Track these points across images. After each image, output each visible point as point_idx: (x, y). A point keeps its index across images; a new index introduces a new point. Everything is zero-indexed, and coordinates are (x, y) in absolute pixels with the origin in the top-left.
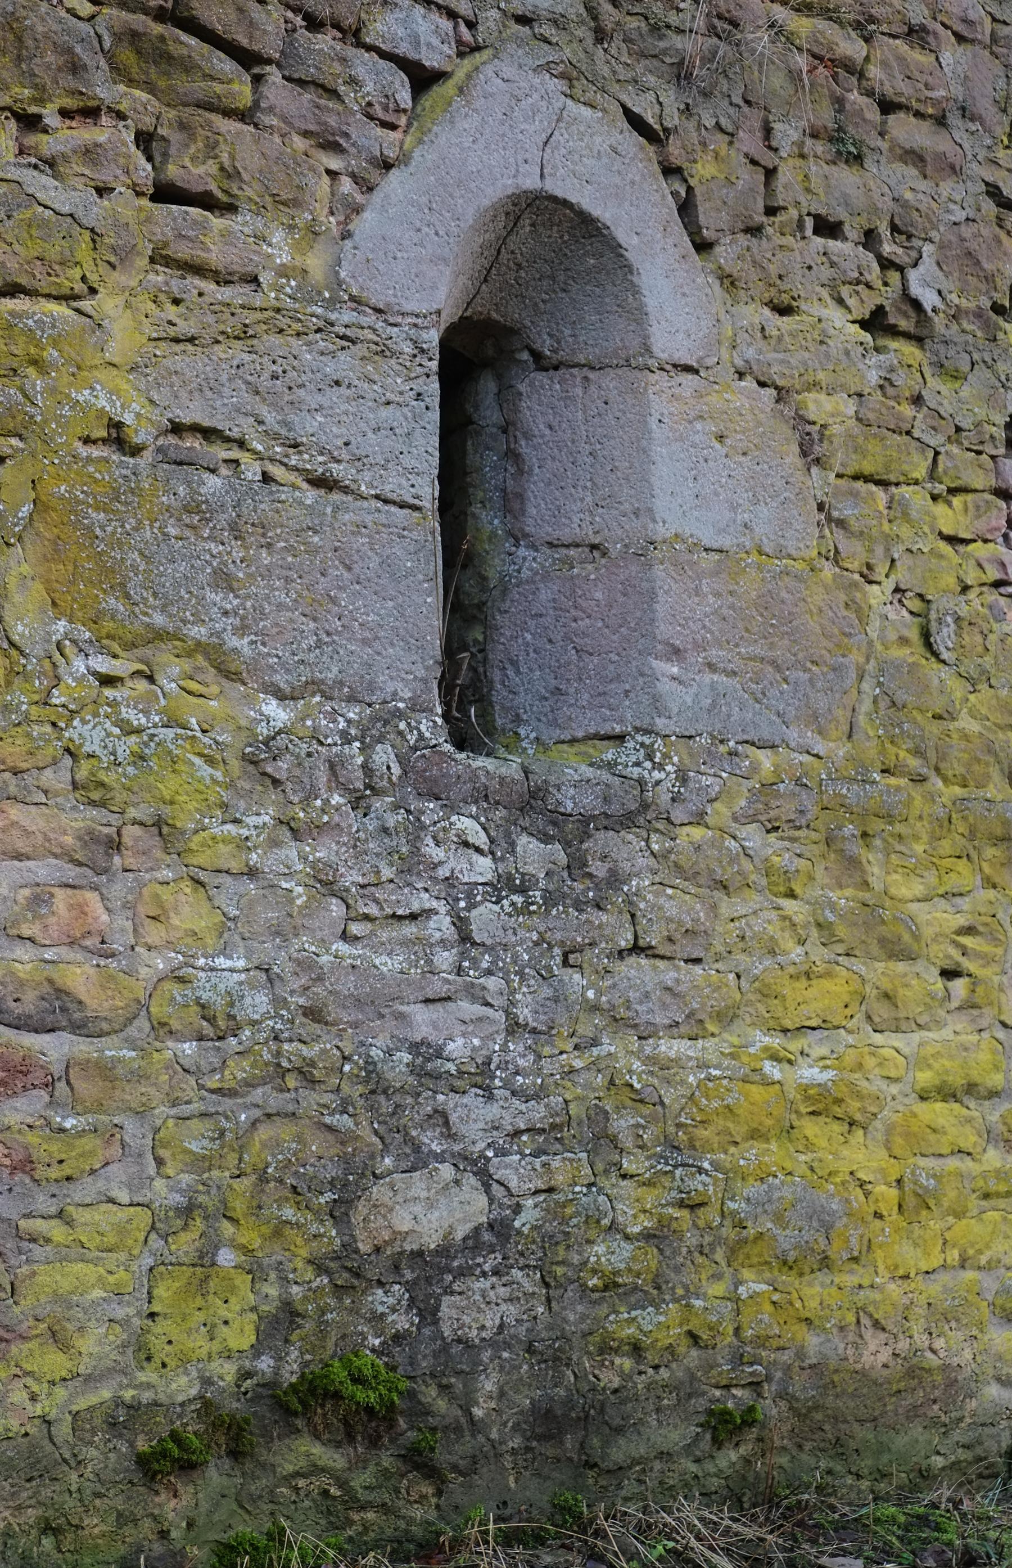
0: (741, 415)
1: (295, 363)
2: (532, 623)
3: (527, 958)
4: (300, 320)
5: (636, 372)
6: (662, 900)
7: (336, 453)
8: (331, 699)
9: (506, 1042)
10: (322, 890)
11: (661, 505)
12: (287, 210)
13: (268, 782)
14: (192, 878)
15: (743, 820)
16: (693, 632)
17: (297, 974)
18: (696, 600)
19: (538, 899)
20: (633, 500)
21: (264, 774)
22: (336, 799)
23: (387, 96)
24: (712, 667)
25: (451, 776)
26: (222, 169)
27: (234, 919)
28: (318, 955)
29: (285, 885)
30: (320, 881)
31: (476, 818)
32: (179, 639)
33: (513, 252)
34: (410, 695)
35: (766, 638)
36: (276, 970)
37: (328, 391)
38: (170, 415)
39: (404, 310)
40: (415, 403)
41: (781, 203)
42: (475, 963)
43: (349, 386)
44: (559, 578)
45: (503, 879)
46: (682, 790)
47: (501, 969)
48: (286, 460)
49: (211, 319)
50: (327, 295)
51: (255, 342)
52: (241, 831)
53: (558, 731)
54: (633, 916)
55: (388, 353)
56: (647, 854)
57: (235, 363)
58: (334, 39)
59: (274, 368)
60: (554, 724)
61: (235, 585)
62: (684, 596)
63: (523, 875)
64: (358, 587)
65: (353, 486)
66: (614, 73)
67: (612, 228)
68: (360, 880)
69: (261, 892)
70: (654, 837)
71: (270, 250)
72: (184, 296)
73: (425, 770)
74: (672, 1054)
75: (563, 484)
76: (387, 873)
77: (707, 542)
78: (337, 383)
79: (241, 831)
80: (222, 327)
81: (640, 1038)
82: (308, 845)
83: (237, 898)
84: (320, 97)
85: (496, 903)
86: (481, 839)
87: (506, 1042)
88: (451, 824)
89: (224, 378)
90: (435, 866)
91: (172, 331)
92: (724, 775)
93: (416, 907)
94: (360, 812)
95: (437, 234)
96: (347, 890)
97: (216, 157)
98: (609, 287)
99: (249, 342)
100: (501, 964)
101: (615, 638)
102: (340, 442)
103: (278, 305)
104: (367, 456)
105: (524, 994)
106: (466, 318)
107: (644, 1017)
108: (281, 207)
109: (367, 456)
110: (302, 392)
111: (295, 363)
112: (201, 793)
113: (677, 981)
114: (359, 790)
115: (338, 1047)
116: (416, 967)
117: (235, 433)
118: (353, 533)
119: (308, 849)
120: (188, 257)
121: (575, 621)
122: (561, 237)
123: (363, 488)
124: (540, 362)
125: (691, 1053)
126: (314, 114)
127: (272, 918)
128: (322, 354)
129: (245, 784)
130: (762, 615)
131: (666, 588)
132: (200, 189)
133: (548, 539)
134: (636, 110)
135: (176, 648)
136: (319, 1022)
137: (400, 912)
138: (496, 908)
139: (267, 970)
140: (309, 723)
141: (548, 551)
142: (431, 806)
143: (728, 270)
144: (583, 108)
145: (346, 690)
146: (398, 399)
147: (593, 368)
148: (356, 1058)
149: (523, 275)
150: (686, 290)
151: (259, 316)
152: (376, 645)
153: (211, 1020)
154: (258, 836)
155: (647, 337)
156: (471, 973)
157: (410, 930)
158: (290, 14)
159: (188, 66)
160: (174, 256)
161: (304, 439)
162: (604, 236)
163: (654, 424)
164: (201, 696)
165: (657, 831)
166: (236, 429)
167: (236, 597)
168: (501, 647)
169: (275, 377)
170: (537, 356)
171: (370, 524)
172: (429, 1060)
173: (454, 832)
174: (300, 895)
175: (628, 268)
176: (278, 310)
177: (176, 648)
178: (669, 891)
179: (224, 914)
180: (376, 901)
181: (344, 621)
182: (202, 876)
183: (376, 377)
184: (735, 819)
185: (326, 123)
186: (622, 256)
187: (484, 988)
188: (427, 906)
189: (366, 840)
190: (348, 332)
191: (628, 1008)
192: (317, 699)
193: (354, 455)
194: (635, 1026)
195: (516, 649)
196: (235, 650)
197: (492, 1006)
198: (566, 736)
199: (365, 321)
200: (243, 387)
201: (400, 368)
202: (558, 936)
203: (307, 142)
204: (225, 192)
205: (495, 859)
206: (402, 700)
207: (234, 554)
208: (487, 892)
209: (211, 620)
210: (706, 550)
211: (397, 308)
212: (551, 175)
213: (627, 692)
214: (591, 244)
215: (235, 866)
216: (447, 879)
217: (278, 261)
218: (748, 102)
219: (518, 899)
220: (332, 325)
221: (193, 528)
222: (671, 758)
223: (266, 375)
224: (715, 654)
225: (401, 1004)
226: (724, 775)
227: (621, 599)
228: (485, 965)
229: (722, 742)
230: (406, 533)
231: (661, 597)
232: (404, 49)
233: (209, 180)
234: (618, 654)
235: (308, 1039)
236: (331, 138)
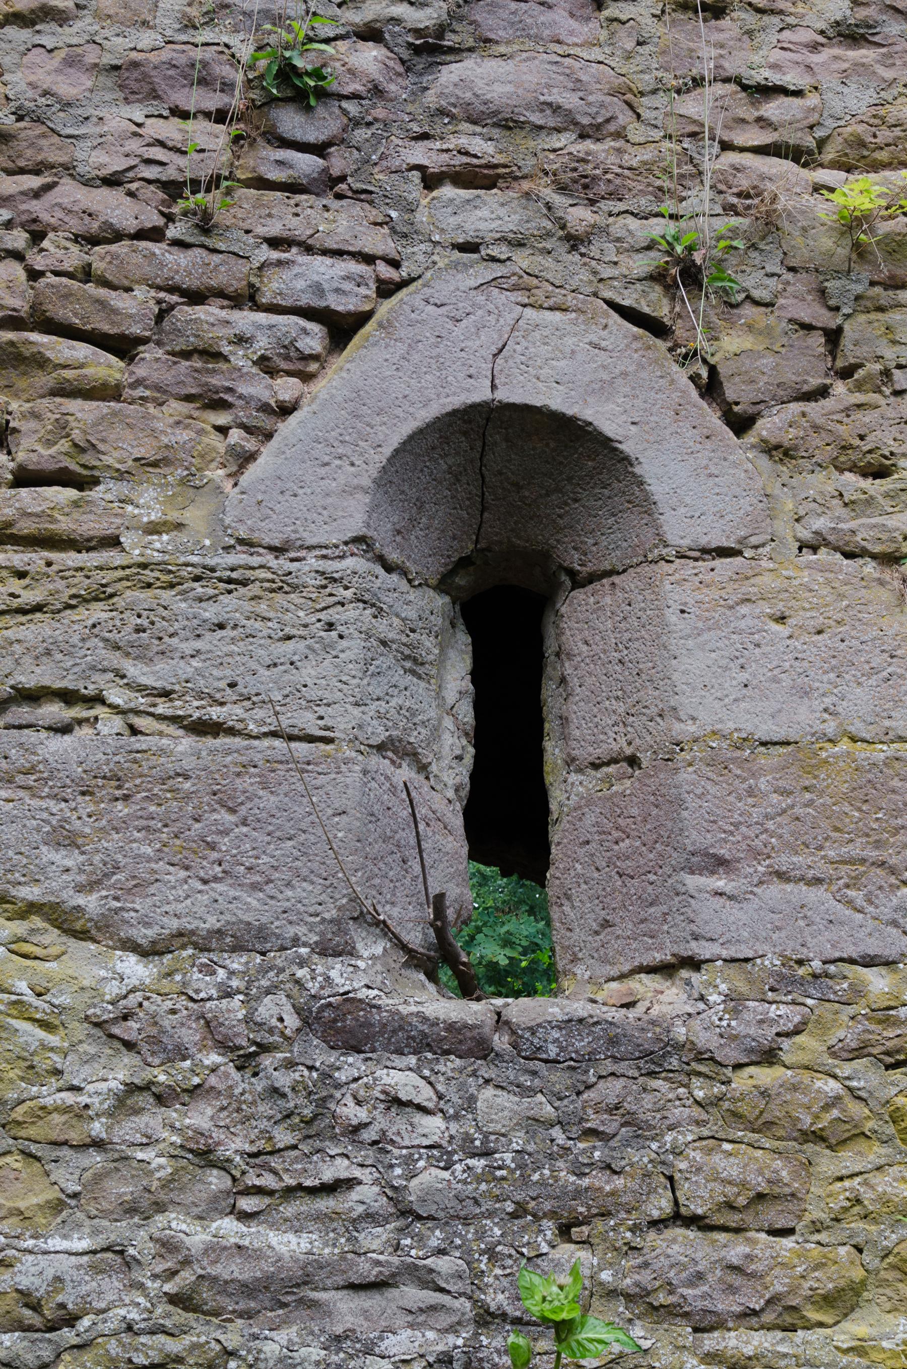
0: (811, 591)
1: (166, 613)
2: (581, 852)
3: (499, 1233)
4: (170, 572)
5: (652, 566)
6: (717, 1158)
7: (218, 696)
8: (209, 950)
9: (476, 1335)
10: (196, 1160)
11: (686, 702)
12: (158, 470)
13: (117, 1045)
14: (22, 1152)
15: (845, 1055)
16: (745, 838)
17: (161, 1256)
18: (750, 800)
19: (508, 1162)
20: (658, 702)
21: (111, 1036)
22: (214, 1058)
23: (285, 347)
24: (782, 876)
25: (373, 1025)
26: (76, 445)
27: (75, 1196)
28: (187, 1235)
29: (140, 1155)
30: (191, 1151)
31: (417, 1070)
32: (8, 902)
33: (500, 473)
34: (316, 938)
35: (868, 835)
36: (131, 1251)
37: (208, 635)
38: (12, 682)
39: (307, 544)
40: (323, 634)
41: (852, 361)
42: (421, 1240)
43: (235, 626)
44: (600, 798)
45: (458, 1142)
46: (733, 1023)
47: (457, 1247)
48: (152, 710)
49: (60, 584)
50: (207, 542)
51: (115, 600)
52: (79, 1099)
53: (608, 967)
54: (671, 1179)
55: (287, 588)
56: (688, 1103)
57: (90, 623)
58: (222, 308)
59: (139, 621)
60: (605, 961)
61: (80, 841)
62: (731, 799)
63: (486, 1135)
64: (245, 829)
65: (239, 726)
66: (595, 273)
67: (595, 423)
68: (248, 1148)
69: (112, 1165)
70: (696, 1082)
71: (136, 511)
72: (28, 568)
73: (335, 1021)
74: (749, 1351)
75: (599, 699)
76: (283, 1137)
77: (762, 733)
78: (221, 626)
79: (79, 1099)
80: (74, 591)
81: (696, 1330)
82: (176, 1110)
83: (78, 1172)
84: (207, 362)
85: (446, 1169)
86: (425, 1095)
87: (476, 1335)
88: (375, 1079)
89: (75, 639)
90: (357, 1129)
91: (15, 603)
92: (810, 1002)
93: (328, 1175)
94: (248, 1073)
95: (353, 464)
96: (229, 1160)
97: (68, 435)
98: (616, 485)
99: (111, 601)
100: (458, 1241)
101: (651, 856)
102: (223, 684)
103: (141, 559)
104: (257, 694)
105: (497, 1277)
106: (483, 550)
107: (700, 1304)
108: (150, 469)
109: (257, 694)
110: (175, 641)
111: (166, 613)
112: (25, 1059)
113: (749, 1257)
114: (242, 1048)
115: (218, 1341)
116: (334, 1245)
117: (91, 691)
118: (238, 775)
119: (174, 1115)
120: (36, 532)
121: (617, 843)
122: (547, 445)
123: (251, 727)
124: (580, 581)
125: (782, 1349)
126: (195, 378)
127: (125, 1193)
128: (201, 600)
129: (89, 1048)
130: (860, 810)
131: (699, 791)
132: (54, 466)
133: (591, 759)
134: (626, 303)
135: (6, 911)
136: (195, 1311)
137: (308, 1183)
138: (446, 1175)
139: (121, 1252)
140: (178, 977)
141: (593, 773)
142: (350, 1060)
143: (773, 441)
144: (547, 313)
145: (228, 940)
146: (302, 632)
147: (618, 573)
148: (244, 1353)
149: (527, 494)
150: (713, 470)
151: (120, 573)
152: (270, 889)
153: (36, 1307)
154: (101, 1103)
155: (658, 527)
156: (413, 1252)
157: (325, 1204)
158: (162, 295)
159: (40, 362)
160: (20, 533)
161: (177, 688)
162: (590, 433)
163: (672, 617)
164: (36, 958)
165: (699, 1074)
166: (91, 687)
167: (83, 853)
168: (557, 882)
169: (139, 630)
170: (572, 573)
171: (260, 763)
172: (351, 1357)
173: (379, 1088)
174: (161, 1167)
175: (626, 460)
176: (144, 566)
177: (6, 911)
178: (727, 1146)
179: (62, 1190)
180: (275, 1173)
181: (225, 866)
182: (33, 1148)
183: (271, 615)
184: (834, 1055)
185: (207, 384)
186: (616, 449)
187: (431, 1271)
188: (344, 1175)
189: (254, 1103)
190: (234, 575)
191: (671, 1293)
192: (190, 951)
193: (241, 695)
194: (686, 1315)
195: (568, 880)
196: (78, 908)
197: (448, 1292)
198: (614, 972)
199: (255, 561)
200: (101, 644)
201: (303, 600)
202: (547, 1206)
203: (192, 405)
204: (84, 466)
205: (446, 1118)
206: (305, 945)
207: (81, 810)
208: (433, 1156)
209: (47, 878)
210: (764, 744)
211: (299, 543)
212: (506, 384)
213: (665, 914)
214: (581, 446)
215: (74, 1136)
216: (375, 1143)
217: (145, 519)
218: (792, 269)
219: (479, 1164)
220: (213, 570)
221: (29, 788)
222: (716, 986)
223: (129, 629)
224: (783, 861)
225: (313, 1290)
226: (810, 1002)
227: (655, 812)
228: (434, 1242)
229: (800, 962)
230: (310, 768)
231: (691, 802)
232: (305, 300)
233: (62, 457)
234: (655, 874)
235: (176, 1332)
236: (216, 397)
